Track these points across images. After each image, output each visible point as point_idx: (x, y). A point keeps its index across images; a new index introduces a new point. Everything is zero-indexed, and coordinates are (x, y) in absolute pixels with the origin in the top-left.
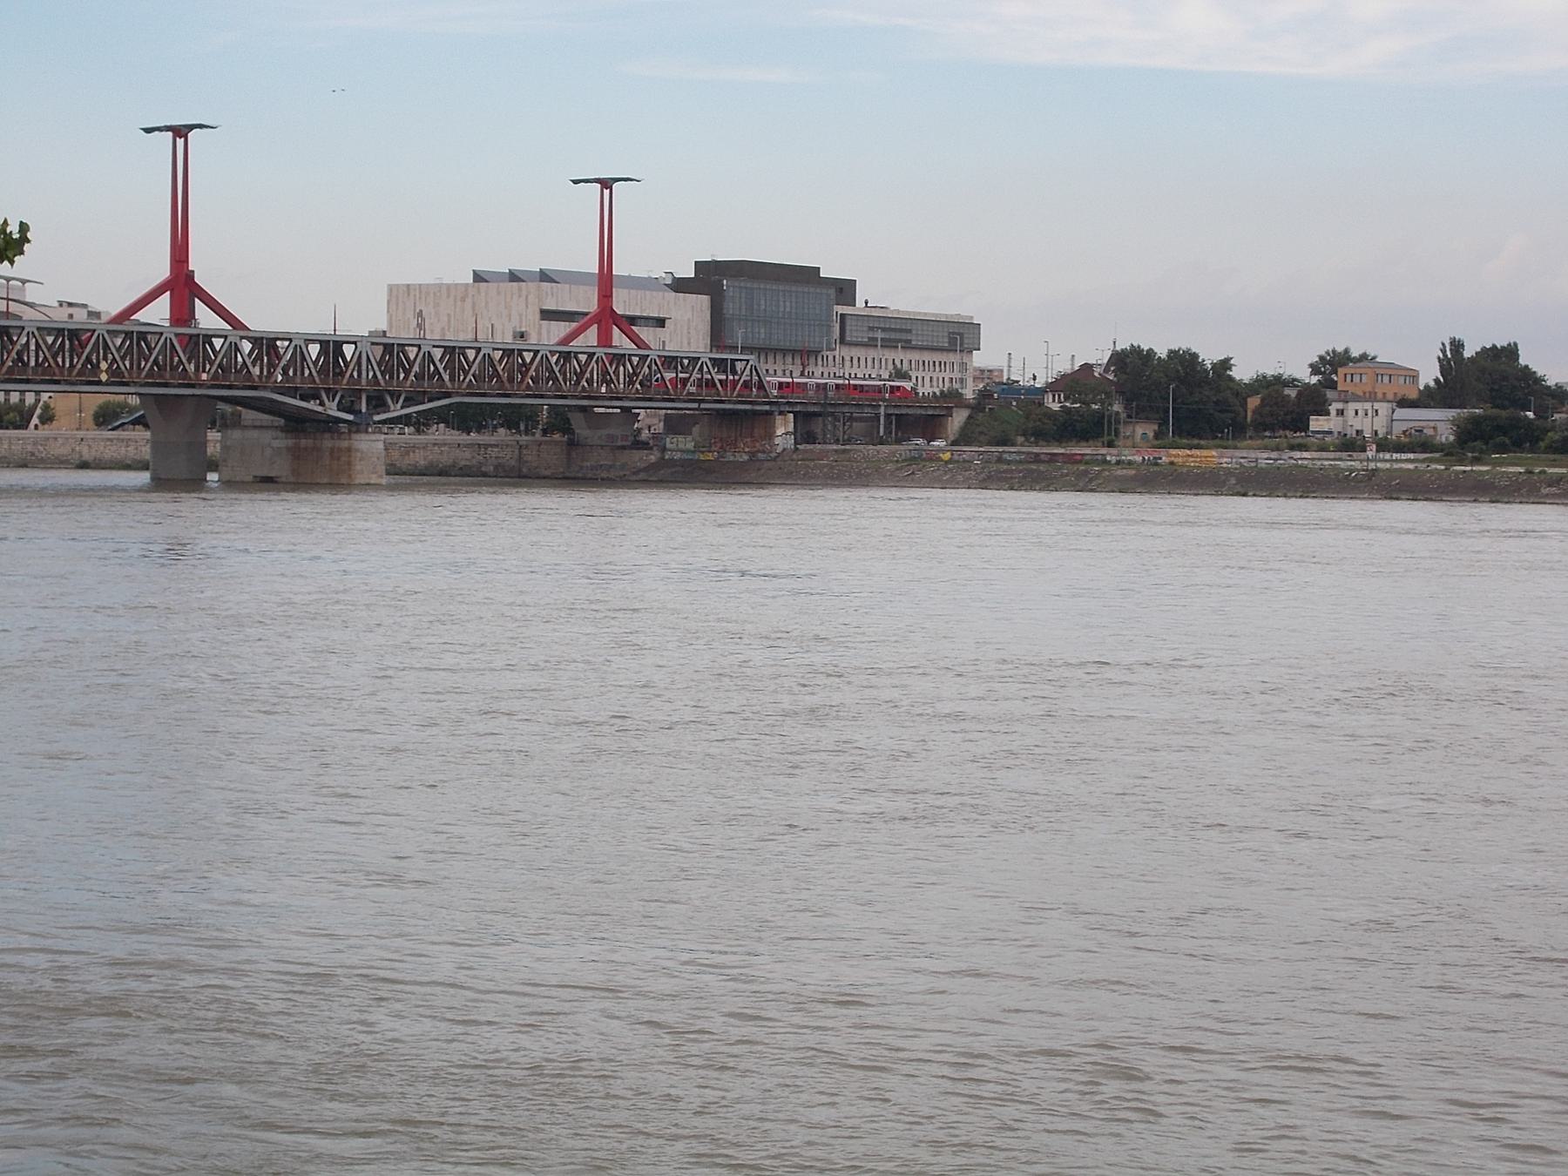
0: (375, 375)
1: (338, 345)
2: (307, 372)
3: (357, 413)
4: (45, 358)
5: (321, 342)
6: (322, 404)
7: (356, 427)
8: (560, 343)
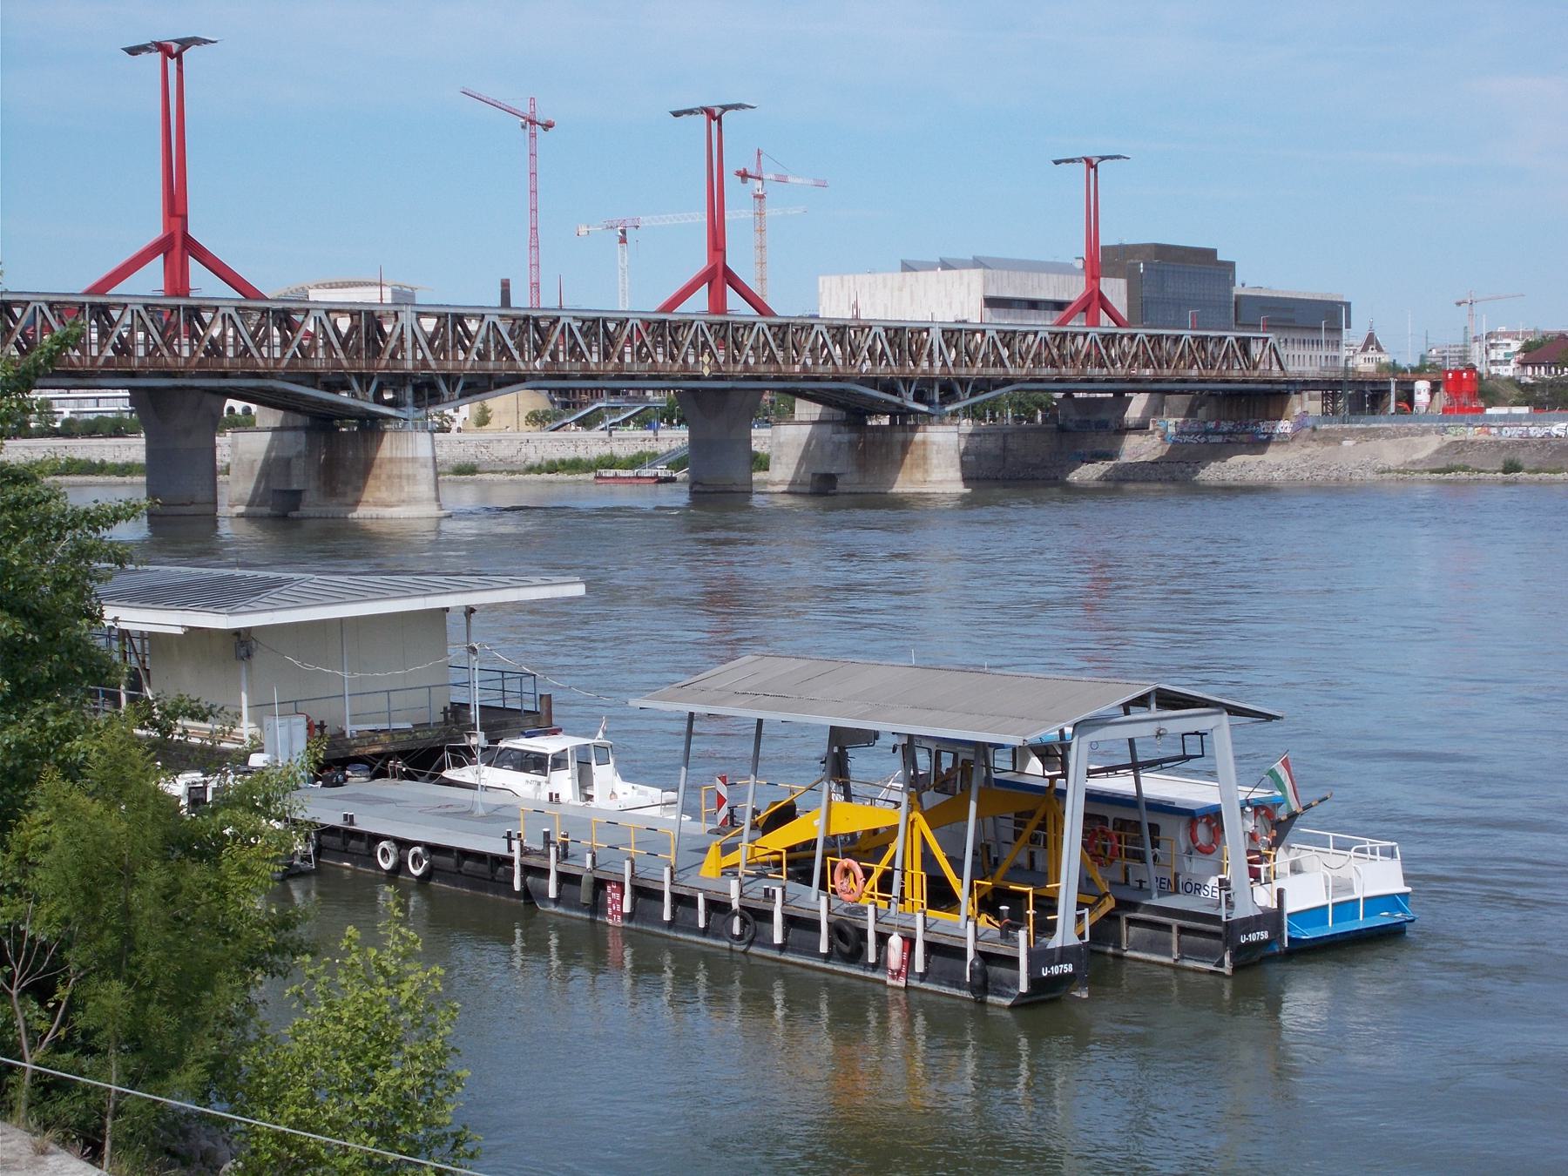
0: (424, 357)
1: (459, 319)
2: (420, 356)
3: (930, 403)
4: (156, 345)
5: (352, 314)
6: (355, 396)
7: (927, 418)
8: (91, 292)
